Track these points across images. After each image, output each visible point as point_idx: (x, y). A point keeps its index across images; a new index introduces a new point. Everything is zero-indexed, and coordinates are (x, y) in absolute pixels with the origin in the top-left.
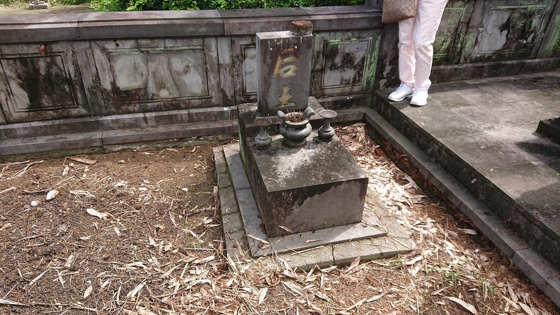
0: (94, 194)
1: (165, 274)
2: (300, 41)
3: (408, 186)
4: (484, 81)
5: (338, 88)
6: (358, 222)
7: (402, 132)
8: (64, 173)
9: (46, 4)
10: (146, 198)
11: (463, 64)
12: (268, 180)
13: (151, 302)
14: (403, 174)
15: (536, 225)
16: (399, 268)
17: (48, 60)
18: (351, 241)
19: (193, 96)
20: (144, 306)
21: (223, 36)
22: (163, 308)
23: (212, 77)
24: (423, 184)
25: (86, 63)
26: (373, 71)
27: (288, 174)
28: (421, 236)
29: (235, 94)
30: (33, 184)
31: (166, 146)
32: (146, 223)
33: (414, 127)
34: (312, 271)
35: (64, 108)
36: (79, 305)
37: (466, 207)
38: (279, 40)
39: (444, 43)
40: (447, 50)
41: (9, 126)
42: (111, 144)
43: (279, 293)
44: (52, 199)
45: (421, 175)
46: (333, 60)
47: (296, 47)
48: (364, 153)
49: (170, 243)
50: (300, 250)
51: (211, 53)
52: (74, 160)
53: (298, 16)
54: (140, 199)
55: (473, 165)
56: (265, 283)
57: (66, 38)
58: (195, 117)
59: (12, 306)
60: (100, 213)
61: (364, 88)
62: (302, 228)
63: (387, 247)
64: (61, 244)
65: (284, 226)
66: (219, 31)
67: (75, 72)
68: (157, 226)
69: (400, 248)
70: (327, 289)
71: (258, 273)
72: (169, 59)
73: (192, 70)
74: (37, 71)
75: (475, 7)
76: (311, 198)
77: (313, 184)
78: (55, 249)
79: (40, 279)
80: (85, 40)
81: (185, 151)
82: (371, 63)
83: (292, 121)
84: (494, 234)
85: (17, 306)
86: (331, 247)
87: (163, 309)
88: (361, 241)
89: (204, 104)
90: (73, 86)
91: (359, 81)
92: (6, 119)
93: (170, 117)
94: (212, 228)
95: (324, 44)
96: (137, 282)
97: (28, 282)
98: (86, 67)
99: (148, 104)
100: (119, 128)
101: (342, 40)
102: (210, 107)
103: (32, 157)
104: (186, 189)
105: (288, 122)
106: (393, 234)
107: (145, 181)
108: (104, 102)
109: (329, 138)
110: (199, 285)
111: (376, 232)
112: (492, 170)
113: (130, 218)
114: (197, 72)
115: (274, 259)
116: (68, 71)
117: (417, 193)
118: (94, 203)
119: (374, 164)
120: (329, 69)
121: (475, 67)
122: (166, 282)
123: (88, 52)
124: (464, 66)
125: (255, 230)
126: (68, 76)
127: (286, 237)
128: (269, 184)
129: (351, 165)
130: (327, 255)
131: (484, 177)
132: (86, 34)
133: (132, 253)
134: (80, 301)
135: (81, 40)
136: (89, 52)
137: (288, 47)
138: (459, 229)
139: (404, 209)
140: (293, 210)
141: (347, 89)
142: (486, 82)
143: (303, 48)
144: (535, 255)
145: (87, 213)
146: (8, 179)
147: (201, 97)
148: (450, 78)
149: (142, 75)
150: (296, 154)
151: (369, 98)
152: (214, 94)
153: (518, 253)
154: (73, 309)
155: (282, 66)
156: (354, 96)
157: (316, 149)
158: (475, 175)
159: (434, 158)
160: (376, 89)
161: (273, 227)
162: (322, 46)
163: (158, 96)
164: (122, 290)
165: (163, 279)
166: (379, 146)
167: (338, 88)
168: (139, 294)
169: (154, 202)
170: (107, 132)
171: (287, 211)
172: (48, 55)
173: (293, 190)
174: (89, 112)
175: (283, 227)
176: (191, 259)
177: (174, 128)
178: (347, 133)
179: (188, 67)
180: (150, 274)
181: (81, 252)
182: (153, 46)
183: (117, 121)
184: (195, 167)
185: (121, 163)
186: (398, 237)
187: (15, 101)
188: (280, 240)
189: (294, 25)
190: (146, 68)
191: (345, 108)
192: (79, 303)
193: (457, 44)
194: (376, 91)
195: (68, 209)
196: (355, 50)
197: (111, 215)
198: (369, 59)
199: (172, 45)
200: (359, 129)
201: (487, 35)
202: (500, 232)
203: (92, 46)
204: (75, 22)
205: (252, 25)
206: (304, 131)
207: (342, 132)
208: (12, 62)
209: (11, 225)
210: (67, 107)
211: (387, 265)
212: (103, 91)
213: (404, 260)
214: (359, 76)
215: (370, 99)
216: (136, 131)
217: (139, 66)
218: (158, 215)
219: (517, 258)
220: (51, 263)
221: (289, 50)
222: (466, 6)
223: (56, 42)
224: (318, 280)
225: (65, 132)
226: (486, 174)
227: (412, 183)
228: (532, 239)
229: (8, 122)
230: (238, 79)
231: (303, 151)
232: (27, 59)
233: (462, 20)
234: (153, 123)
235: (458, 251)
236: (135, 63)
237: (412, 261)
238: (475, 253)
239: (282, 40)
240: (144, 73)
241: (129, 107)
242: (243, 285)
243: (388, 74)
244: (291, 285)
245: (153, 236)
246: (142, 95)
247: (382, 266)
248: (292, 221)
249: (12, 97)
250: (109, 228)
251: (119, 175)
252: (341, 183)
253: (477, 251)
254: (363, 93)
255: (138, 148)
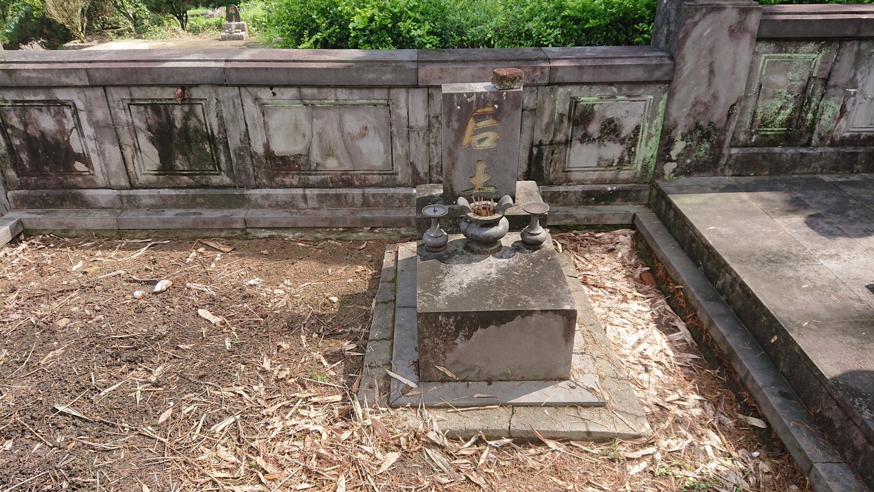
0: (216, 291)
1: (268, 410)
2: (503, 97)
3: (676, 336)
4: (856, 178)
5: (594, 171)
6: (562, 379)
7: (686, 248)
8: (188, 260)
9: (242, 33)
10: (279, 305)
11: (817, 146)
12: (424, 296)
13: (238, 444)
14: (673, 317)
15: (856, 425)
16: (612, 460)
17: (186, 108)
18: (544, 406)
19: (371, 171)
20: (227, 447)
21: (416, 86)
22: (251, 453)
23: (398, 144)
24: (701, 337)
25: (233, 116)
26: (653, 148)
27: (455, 290)
28: (670, 419)
29: (430, 171)
30: (147, 270)
31: (328, 237)
32: (268, 337)
33: (702, 243)
34: (473, 440)
35: (203, 173)
36: (148, 430)
37: (753, 381)
38: (470, 95)
39: (782, 111)
40: (788, 122)
41: (133, 192)
42: (256, 228)
43: (415, 463)
44: (161, 292)
45: (699, 321)
46: (585, 128)
47: (496, 106)
48: (620, 277)
49: (288, 369)
50: (461, 407)
51: (399, 111)
52: (206, 245)
53: (531, 60)
54: (270, 306)
55: (775, 313)
56: (399, 446)
57: (209, 81)
58: (371, 199)
59: (74, 417)
60: (213, 317)
61: (638, 175)
62: (472, 375)
63: (600, 424)
64: (153, 350)
65: (444, 367)
66: (410, 79)
67: (219, 128)
68: (280, 343)
69: (621, 429)
70: (488, 470)
71: (391, 430)
72: (341, 116)
73: (371, 133)
74: (171, 122)
75: (840, 53)
76: (483, 330)
77: (487, 309)
78: (143, 355)
79: (114, 390)
80: (233, 86)
81: (352, 246)
82: (650, 136)
83: (478, 214)
84: (787, 430)
85: (80, 418)
86: (511, 409)
87: (249, 455)
88: (560, 408)
89: (386, 182)
90: (215, 146)
91: (629, 163)
92: (130, 182)
93: (338, 197)
94: (352, 357)
95: (571, 103)
96: (228, 414)
97: (100, 392)
98: (233, 121)
99: (310, 177)
100: (270, 206)
101: (601, 98)
102: (394, 187)
103: (156, 235)
104: (335, 299)
105: (470, 215)
106: (616, 406)
107: (286, 282)
108: (254, 171)
109: (536, 245)
110: (307, 432)
111: (589, 398)
112: (806, 323)
113: (249, 328)
114: (378, 137)
115: (421, 413)
116: (211, 125)
117: (688, 349)
118: (212, 303)
119: (630, 296)
120: (578, 142)
121: (838, 153)
122: (266, 420)
123: (236, 100)
124: (819, 150)
125: (406, 367)
126: (210, 131)
127: (446, 385)
128: (424, 301)
129: (557, 288)
130: (500, 421)
131: (788, 334)
132: (234, 77)
133: (236, 375)
134: (153, 426)
135: (227, 85)
136: (238, 101)
137: (485, 106)
138: (740, 416)
139: (657, 371)
140: (456, 344)
141: (609, 174)
142: (859, 179)
143: (507, 108)
144: (850, 476)
145: (198, 314)
146: (119, 260)
147: (383, 172)
148: (793, 169)
149: (304, 136)
150: (478, 263)
151: (646, 190)
152: (400, 169)
153: (818, 467)
154: (140, 434)
155: (476, 132)
156: (621, 185)
157: (511, 259)
158: (777, 330)
159: (724, 296)
160: (658, 177)
161: (427, 365)
162: (567, 108)
163: (324, 166)
164: (205, 421)
165: (264, 416)
166: (648, 268)
167: (594, 171)
168: (226, 429)
169: (288, 311)
170: (254, 210)
171: (447, 344)
172: (186, 102)
173: (456, 314)
174: (234, 181)
175: (441, 369)
176: (308, 395)
177: (341, 212)
178: (600, 244)
179: (366, 128)
180: (248, 405)
181: (174, 363)
182: (320, 98)
183: (267, 197)
184: (358, 270)
185: (262, 254)
186: (624, 412)
187: (142, 160)
188: (435, 388)
189: (496, 73)
190: (310, 126)
191: (603, 203)
192: (149, 428)
193: (807, 113)
194: (657, 181)
195: (178, 306)
196: (623, 113)
197: (226, 321)
198: (646, 129)
199: (346, 97)
200: (622, 238)
201: (864, 100)
202: (798, 428)
203: (242, 94)
204: (221, 61)
205: (458, 72)
206: (493, 231)
207: (594, 241)
208: (142, 108)
209: (103, 318)
210: (207, 172)
211: (595, 451)
212: (254, 154)
213: (624, 450)
214: (629, 156)
215: (647, 193)
216: (291, 212)
217: (300, 124)
218: (286, 329)
219: (816, 475)
220: (133, 372)
221: (486, 110)
222: (823, 52)
223: (197, 85)
224: (477, 455)
225: (202, 205)
226: (792, 330)
227: (683, 333)
228: (849, 449)
229: (132, 187)
230: (436, 149)
231: (491, 259)
232: (160, 106)
233: (814, 75)
234: (315, 203)
235: (724, 450)
236: (296, 120)
237: (637, 453)
238: (752, 458)
239: (475, 95)
240: (307, 134)
241: (285, 180)
242: (364, 442)
243: (679, 155)
244: (436, 455)
245: (270, 356)
246: (302, 164)
247: (587, 452)
248: (457, 362)
249: (139, 154)
250: (219, 337)
251: (256, 269)
252: (530, 313)
253: (756, 454)
254: (635, 183)
255: (291, 236)
